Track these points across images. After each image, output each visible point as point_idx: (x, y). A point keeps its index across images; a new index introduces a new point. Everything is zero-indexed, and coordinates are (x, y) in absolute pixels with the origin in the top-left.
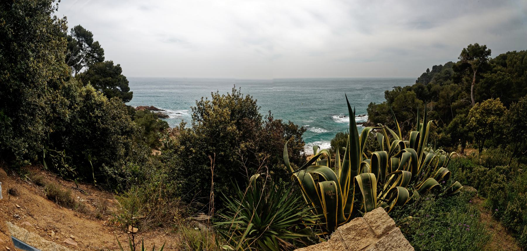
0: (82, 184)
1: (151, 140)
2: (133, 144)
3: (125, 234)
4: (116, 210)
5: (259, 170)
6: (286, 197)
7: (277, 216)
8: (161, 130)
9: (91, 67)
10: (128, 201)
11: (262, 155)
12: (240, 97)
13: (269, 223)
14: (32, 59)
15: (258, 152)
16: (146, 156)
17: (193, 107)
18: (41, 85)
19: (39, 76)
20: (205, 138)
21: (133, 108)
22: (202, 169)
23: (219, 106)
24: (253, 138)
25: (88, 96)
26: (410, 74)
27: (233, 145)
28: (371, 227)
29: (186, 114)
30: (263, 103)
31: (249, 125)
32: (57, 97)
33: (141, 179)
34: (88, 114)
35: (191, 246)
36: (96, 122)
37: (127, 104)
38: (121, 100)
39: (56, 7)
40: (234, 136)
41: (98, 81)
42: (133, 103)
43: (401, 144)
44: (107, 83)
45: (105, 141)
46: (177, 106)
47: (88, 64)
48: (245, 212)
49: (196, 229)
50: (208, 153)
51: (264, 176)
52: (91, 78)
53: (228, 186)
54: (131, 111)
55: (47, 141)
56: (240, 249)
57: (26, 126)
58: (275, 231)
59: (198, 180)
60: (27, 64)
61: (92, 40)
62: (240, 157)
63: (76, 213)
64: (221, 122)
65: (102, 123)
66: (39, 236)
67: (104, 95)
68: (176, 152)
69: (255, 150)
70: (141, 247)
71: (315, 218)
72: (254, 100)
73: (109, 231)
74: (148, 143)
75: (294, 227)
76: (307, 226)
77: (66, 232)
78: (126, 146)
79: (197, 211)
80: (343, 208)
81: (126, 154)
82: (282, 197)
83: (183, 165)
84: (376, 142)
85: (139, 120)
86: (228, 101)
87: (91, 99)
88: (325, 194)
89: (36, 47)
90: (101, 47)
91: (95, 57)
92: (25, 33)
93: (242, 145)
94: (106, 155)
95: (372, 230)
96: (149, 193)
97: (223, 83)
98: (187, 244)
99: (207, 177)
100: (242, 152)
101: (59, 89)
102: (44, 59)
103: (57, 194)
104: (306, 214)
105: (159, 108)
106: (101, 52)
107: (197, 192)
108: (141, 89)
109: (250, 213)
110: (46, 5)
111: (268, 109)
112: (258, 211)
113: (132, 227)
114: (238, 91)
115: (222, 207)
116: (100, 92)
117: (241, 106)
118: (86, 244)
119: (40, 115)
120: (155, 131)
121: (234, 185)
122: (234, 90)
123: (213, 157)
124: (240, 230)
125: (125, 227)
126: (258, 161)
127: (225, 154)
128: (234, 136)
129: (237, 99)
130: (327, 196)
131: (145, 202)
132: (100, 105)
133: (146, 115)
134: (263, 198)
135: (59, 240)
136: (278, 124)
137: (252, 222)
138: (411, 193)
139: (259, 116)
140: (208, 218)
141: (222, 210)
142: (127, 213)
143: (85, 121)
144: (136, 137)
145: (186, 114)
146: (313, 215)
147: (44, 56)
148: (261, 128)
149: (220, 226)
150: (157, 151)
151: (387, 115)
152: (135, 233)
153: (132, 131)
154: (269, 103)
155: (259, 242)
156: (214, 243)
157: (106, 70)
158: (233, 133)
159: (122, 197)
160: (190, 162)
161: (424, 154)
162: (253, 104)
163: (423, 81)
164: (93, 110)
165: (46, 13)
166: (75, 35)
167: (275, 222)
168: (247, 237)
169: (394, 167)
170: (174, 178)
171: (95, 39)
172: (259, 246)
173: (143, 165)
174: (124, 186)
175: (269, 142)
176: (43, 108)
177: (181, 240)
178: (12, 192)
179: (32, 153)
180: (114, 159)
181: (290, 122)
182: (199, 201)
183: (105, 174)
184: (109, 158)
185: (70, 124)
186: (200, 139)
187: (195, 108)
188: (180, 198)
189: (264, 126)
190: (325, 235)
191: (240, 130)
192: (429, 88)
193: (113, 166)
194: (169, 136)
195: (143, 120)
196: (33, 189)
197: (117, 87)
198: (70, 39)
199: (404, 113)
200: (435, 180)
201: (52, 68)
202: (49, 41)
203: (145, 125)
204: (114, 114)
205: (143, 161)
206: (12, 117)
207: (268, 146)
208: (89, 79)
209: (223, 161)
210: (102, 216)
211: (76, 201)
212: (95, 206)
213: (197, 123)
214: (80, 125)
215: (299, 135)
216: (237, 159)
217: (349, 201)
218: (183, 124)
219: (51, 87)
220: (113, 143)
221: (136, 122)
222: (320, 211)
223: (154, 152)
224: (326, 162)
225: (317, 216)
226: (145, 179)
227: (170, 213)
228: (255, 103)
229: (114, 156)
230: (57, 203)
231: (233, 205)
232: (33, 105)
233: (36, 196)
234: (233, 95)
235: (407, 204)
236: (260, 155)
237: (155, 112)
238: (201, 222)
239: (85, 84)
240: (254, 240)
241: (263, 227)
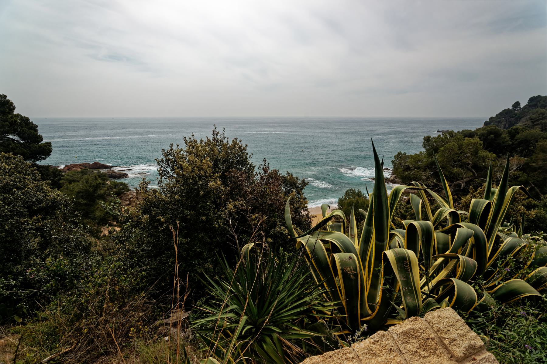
5: (253, 238)
6: (289, 274)
7: (278, 302)
8: (119, 194)
11: (256, 218)
12: (225, 141)
13: (268, 314)
15: (251, 213)
17: (159, 159)
20: (179, 200)
24: (244, 196)
26: (474, 110)
27: (218, 206)
28: (441, 339)
30: (255, 149)
31: (238, 178)
40: (218, 194)
42: (56, 160)
43: (452, 214)
48: (236, 299)
51: (259, 245)
53: (212, 262)
54: (53, 176)
56: (229, 361)
58: (277, 326)
62: (228, 222)
64: (200, 177)
69: (246, 211)
71: (330, 306)
72: (244, 145)
75: (302, 321)
76: (320, 318)
80: (366, 294)
81: (43, 246)
82: (284, 274)
84: (408, 206)
85: (71, 186)
88: (342, 270)
93: (230, 206)
95: (444, 344)
97: (202, 124)
100: (230, 214)
104: (317, 299)
105: (108, 165)
109: (242, 299)
111: (261, 157)
112: (253, 297)
114: (221, 133)
115: (203, 295)
117: (226, 154)
121: (220, 260)
122: (215, 133)
123: (175, 228)
124: (230, 329)
126: (251, 225)
127: (207, 219)
128: (218, 194)
129: (220, 144)
130: (345, 275)
133: (86, 176)
134: (259, 276)
136: (274, 175)
137: (246, 314)
138: (480, 296)
139: (251, 166)
141: (204, 299)
146: (326, 302)
148: (254, 182)
149: (202, 326)
151: (425, 170)
153: (54, 206)
154: (263, 149)
155: (256, 347)
158: (217, 190)
159: (29, 325)
161: (497, 236)
162: (243, 150)
163: (499, 122)
167: (276, 312)
168: (239, 339)
169: (440, 246)
172: (256, 354)
175: (265, 200)
181: (288, 173)
186: (171, 202)
187: (162, 160)
189: (257, 179)
190: (347, 335)
191: (226, 185)
192: (513, 134)
199: (455, 170)
200: (528, 285)
207: (264, 205)
215: (299, 190)
216: (224, 224)
217: (374, 286)
222: (335, 296)
224: (340, 226)
225: (332, 304)
228: (244, 149)
231: (219, 290)
234: (215, 140)
235: (475, 309)
236: (254, 217)
237: (103, 171)
240: (249, 342)
241: (261, 320)
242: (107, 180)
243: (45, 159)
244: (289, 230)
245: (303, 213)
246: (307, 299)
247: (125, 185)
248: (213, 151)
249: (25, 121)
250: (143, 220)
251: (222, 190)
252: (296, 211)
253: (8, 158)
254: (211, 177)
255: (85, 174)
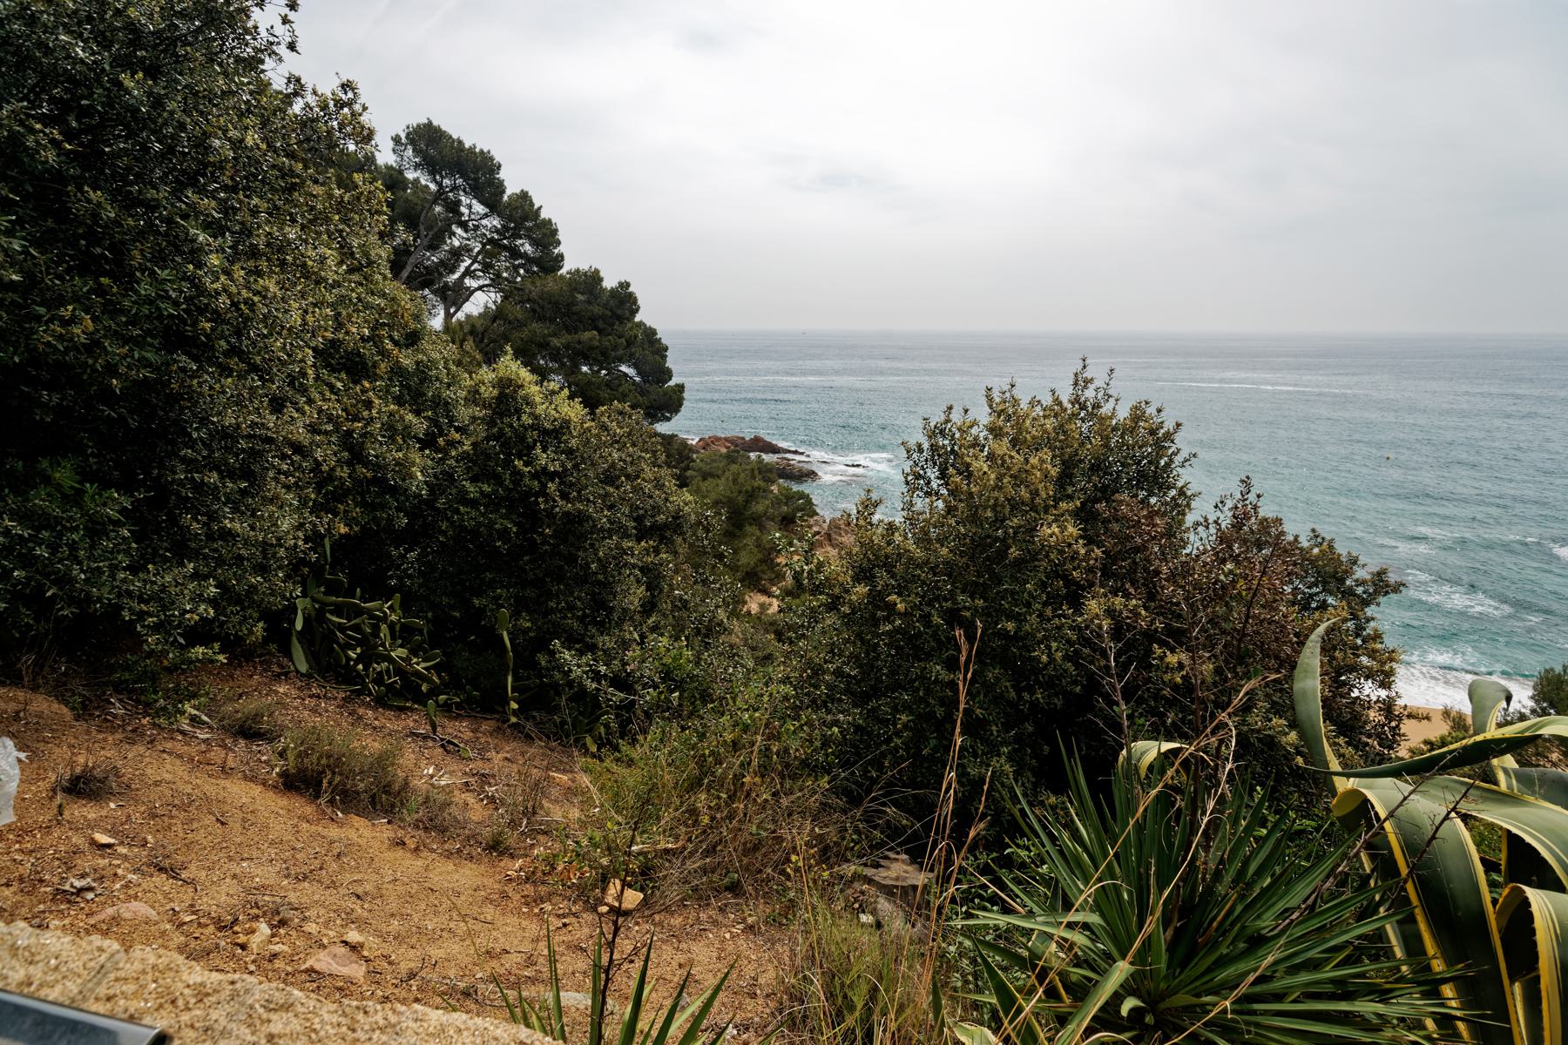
0: (458, 717)
1: (746, 559)
2: (676, 572)
3: (588, 917)
4: (575, 813)
8: (787, 522)
9: (510, 293)
10: (631, 782)
12: (1106, 409)
14: (214, 260)
16: (722, 614)
17: (912, 443)
18: (284, 363)
19: (272, 328)
20: (946, 563)
21: (684, 443)
22: (922, 678)
23: (1014, 442)
25: (507, 399)
29: (884, 469)
32: (369, 404)
33: (690, 696)
34: (508, 463)
35: (830, 996)
36: (537, 494)
37: (662, 428)
38: (638, 415)
39: (280, 30)
41: (543, 346)
42: (685, 426)
44: (584, 354)
45: (572, 560)
46: (850, 439)
47: (496, 282)
49: (864, 918)
50: (953, 617)
52: (515, 335)
54: (677, 453)
55: (317, 569)
57: (213, 517)
59: (904, 718)
60: (194, 281)
61: (500, 187)
63: (400, 833)
64: (1015, 505)
65: (564, 496)
66: (180, 959)
67: (571, 397)
68: (833, 606)
70: (636, 976)
72: (1169, 425)
73: (528, 901)
74: (733, 568)
77: (326, 924)
78: (652, 578)
79: (881, 845)
81: (649, 607)
83: (854, 657)
85: (705, 486)
86: (1050, 424)
87: (518, 412)
89: (227, 210)
90: (544, 215)
91: (524, 255)
92: (145, 149)
93: (1093, 606)
94: (571, 608)
96: (712, 753)
97: (1038, 351)
98: (817, 982)
99: (940, 712)
101: (373, 378)
102: (283, 263)
103: (335, 763)
105: (783, 444)
106: (546, 235)
107: (892, 767)
108: (715, 373)
110: (233, 20)
113: (625, 884)
114: (1099, 383)
116: (553, 386)
118: (404, 967)
119: (287, 474)
120: (761, 527)
122: (1081, 382)
123: (970, 638)
125: (595, 886)
127: (1019, 629)
129: (1091, 415)
131: (694, 785)
132: (555, 434)
133: (734, 467)
135: (278, 964)
139: (1182, 492)
140: (920, 879)
142: (617, 826)
143: (495, 492)
144: (691, 546)
145: (883, 467)
147: (281, 250)
150: (763, 599)
152: (627, 913)
153: (677, 523)
156: (925, 1001)
157: (574, 303)
158: (1061, 552)
159: (608, 763)
160: (883, 647)
162: (1161, 440)
164: (526, 452)
165: (238, 60)
166: (417, 167)
170: (814, 701)
171: (513, 181)
173: (707, 646)
174: (624, 726)
176: (298, 448)
177: (798, 961)
178: (82, 787)
179: (236, 619)
180: (602, 624)
182: (895, 803)
183: (557, 675)
184: (582, 620)
185: (430, 503)
186: (927, 562)
188: (824, 782)
191: (1090, 541)
193: (592, 648)
194: (813, 546)
195: (721, 487)
196: (217, 754)
197: (624, 368)
198: (394, 180)
201: (330, 298)
202: (292, 188)
203: (730, 503)
204: (613, 465)
205: (708, 632)
206: (127, 487)
208: (507, 340)
209: (1008, 654)
210: (511, 839)
211: (418, 783)
212: (492, 800)
213: (920, 503)
214: (474, 503)
215: (1358, 603)
216: (1066, 658)
218: (869, 505)
219: (333, 370)
220: (603, 565)
221: (696, 492)
223: (754, 603)
226: (706, 697)
227: (780, 840)
228: (1169, 437)
229: (601, 612)
230: (322, 801)
232: (249, 436)
233: (226, 783)
234: (1075, 401)
237: (768, 458)
238: (889, 891)
239: (491, 358)
242: (773, 482)
243: (669, 419)
244: (1301, 736)
245: (1369, 690)
246: (1366, 1007)
247: (807, 498)
248: (1065, 432)
249: (650, 333)
250: (854, 598)
251: (1077, 552)
252: (1337, 676)
253: (621, 413)
254: (1046, 510)
255: (734, 462)
